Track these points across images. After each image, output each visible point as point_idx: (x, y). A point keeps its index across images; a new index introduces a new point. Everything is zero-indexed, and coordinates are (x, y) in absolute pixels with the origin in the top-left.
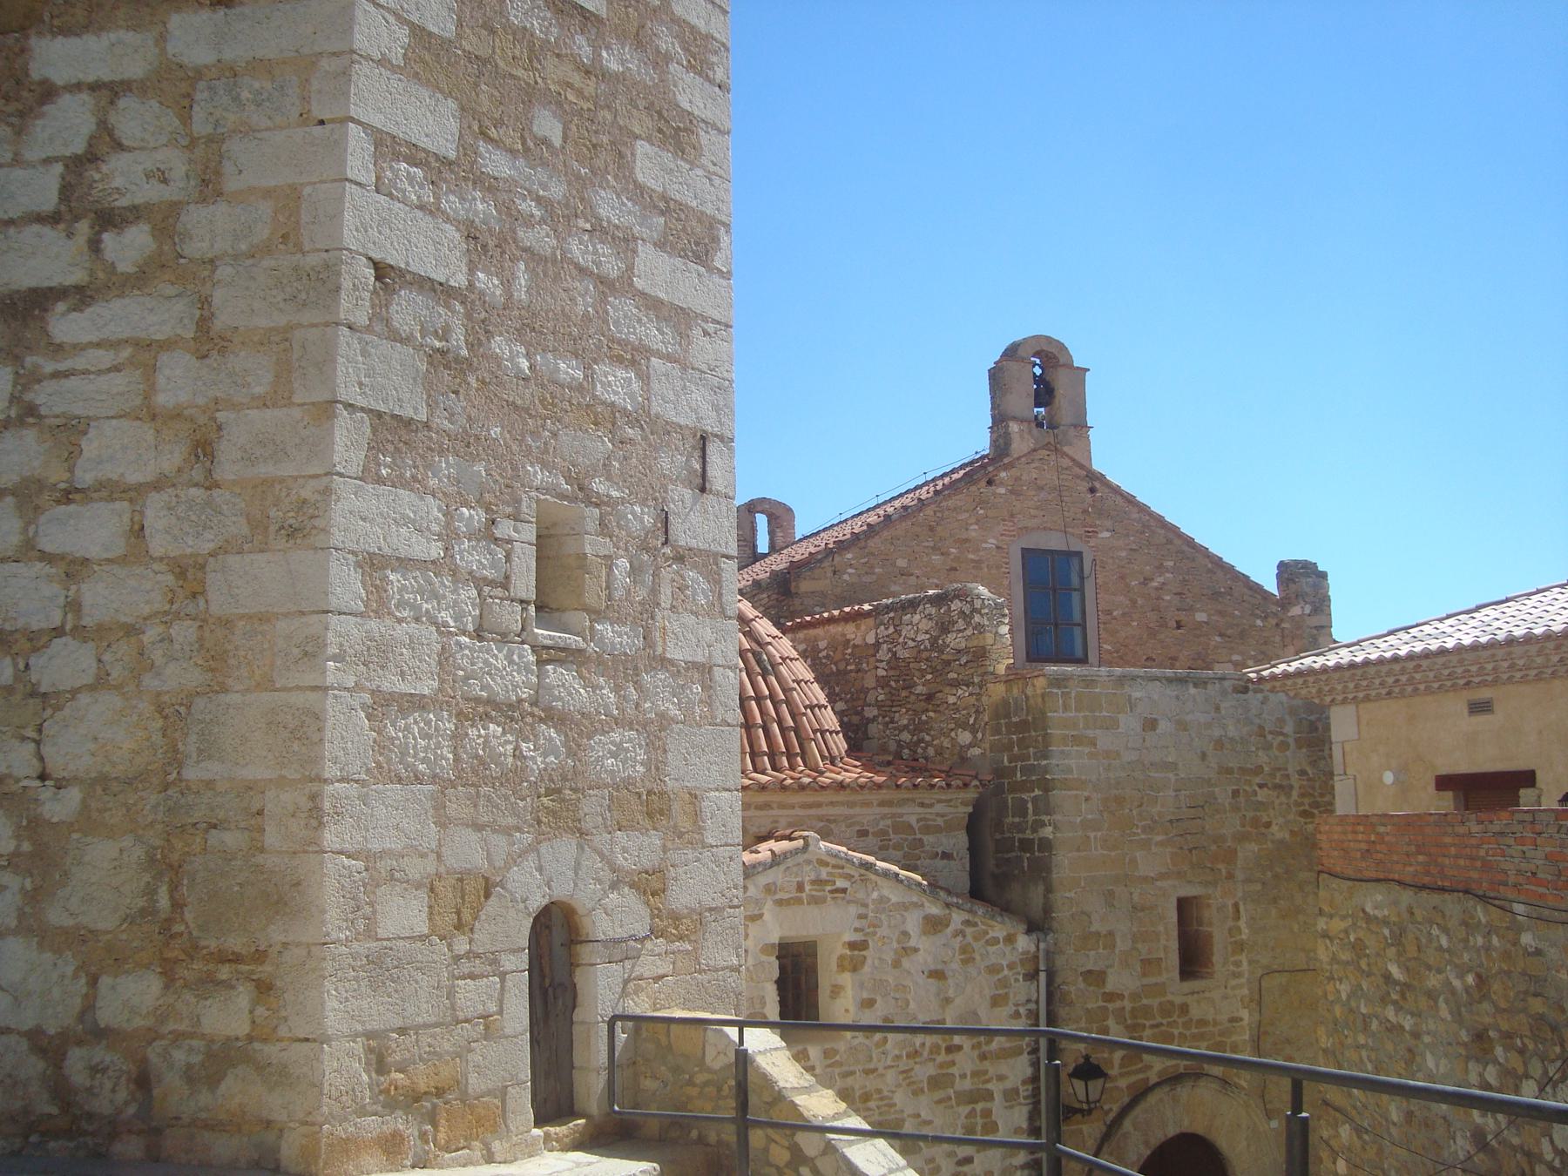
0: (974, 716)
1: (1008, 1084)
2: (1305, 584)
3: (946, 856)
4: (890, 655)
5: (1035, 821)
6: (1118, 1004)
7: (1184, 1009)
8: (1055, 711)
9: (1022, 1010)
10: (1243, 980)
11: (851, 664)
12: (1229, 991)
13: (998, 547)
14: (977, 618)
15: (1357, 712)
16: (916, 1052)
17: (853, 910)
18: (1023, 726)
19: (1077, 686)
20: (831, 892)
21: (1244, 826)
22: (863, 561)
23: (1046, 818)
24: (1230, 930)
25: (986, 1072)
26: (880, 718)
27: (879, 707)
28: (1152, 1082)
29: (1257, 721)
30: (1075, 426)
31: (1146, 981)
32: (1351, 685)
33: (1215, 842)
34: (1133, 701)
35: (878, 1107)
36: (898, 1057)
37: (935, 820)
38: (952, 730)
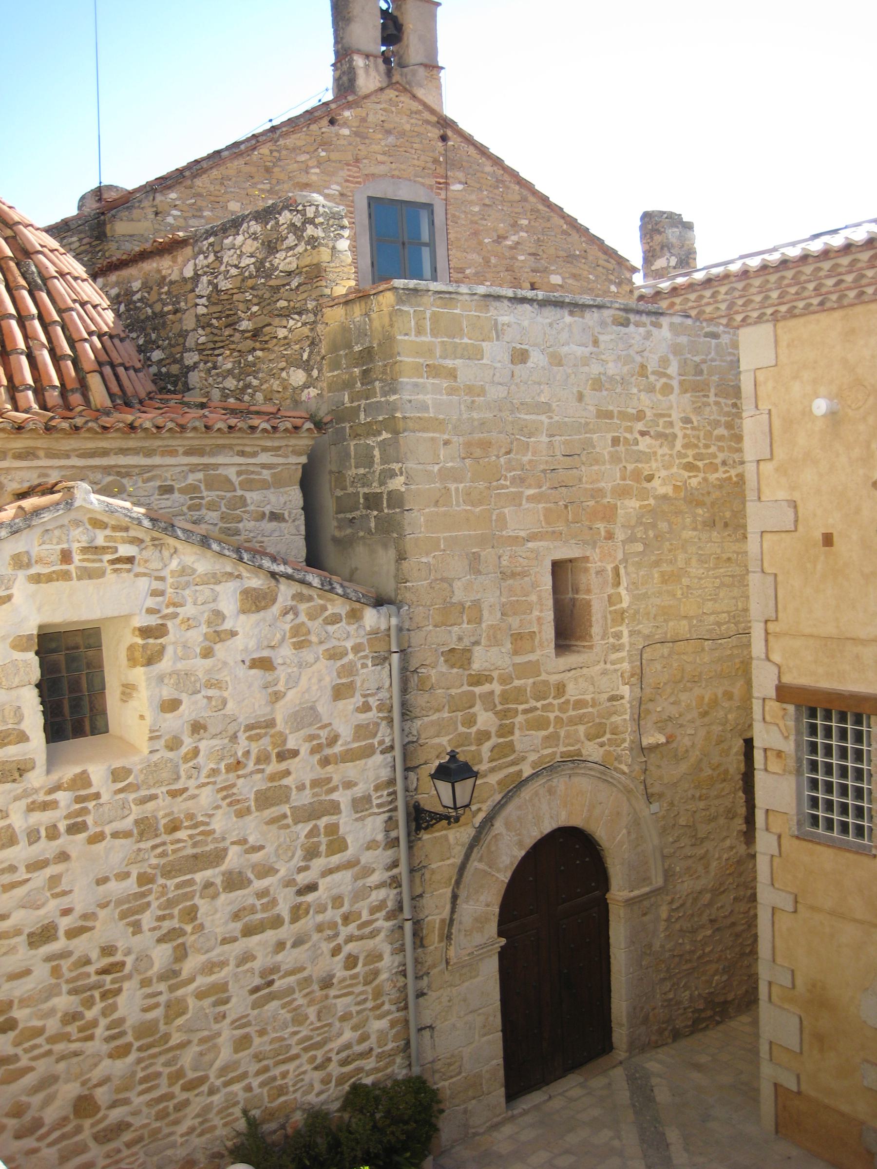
0: (308, 350)
1: (359, 791)
2: (672, 234)
3: (275, 517)
4: (211, 288)
5: (382, 471)
6: (486, 688)
7: (561, 689)
8: (406, 334)
9: (373, 702)
10: (624, 654)
11: (168, 304)
12: (608, 666)
13: (342, 195)
14: (310, 230)
15: (775, 331)
16: (239, 763)
17: (144, 584)
18: (368, 354)
19: (432, 305)
20: (113, 562)
21: (624, 479)
22: (188, 202)
23: (396, 466)
24: (610, 597)
25: (329, 780)
26: (202, 364)
27: (200, 351)
28: (526, 774)
29: (638, 359)
30: (426, 66)
31: (518, 660)
32: (774, 295)
33: (593, 497)
34: (500, 327)
35: (191, 837)
36: (214, 772)
37: (259, 474)
38: (283, 369)
